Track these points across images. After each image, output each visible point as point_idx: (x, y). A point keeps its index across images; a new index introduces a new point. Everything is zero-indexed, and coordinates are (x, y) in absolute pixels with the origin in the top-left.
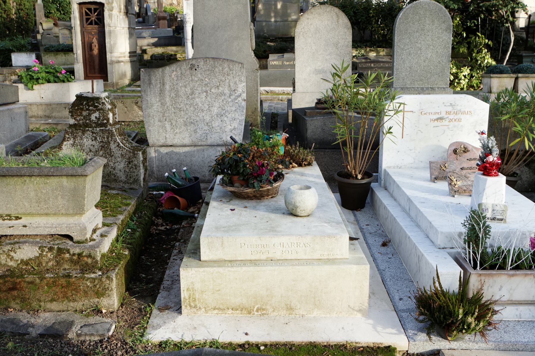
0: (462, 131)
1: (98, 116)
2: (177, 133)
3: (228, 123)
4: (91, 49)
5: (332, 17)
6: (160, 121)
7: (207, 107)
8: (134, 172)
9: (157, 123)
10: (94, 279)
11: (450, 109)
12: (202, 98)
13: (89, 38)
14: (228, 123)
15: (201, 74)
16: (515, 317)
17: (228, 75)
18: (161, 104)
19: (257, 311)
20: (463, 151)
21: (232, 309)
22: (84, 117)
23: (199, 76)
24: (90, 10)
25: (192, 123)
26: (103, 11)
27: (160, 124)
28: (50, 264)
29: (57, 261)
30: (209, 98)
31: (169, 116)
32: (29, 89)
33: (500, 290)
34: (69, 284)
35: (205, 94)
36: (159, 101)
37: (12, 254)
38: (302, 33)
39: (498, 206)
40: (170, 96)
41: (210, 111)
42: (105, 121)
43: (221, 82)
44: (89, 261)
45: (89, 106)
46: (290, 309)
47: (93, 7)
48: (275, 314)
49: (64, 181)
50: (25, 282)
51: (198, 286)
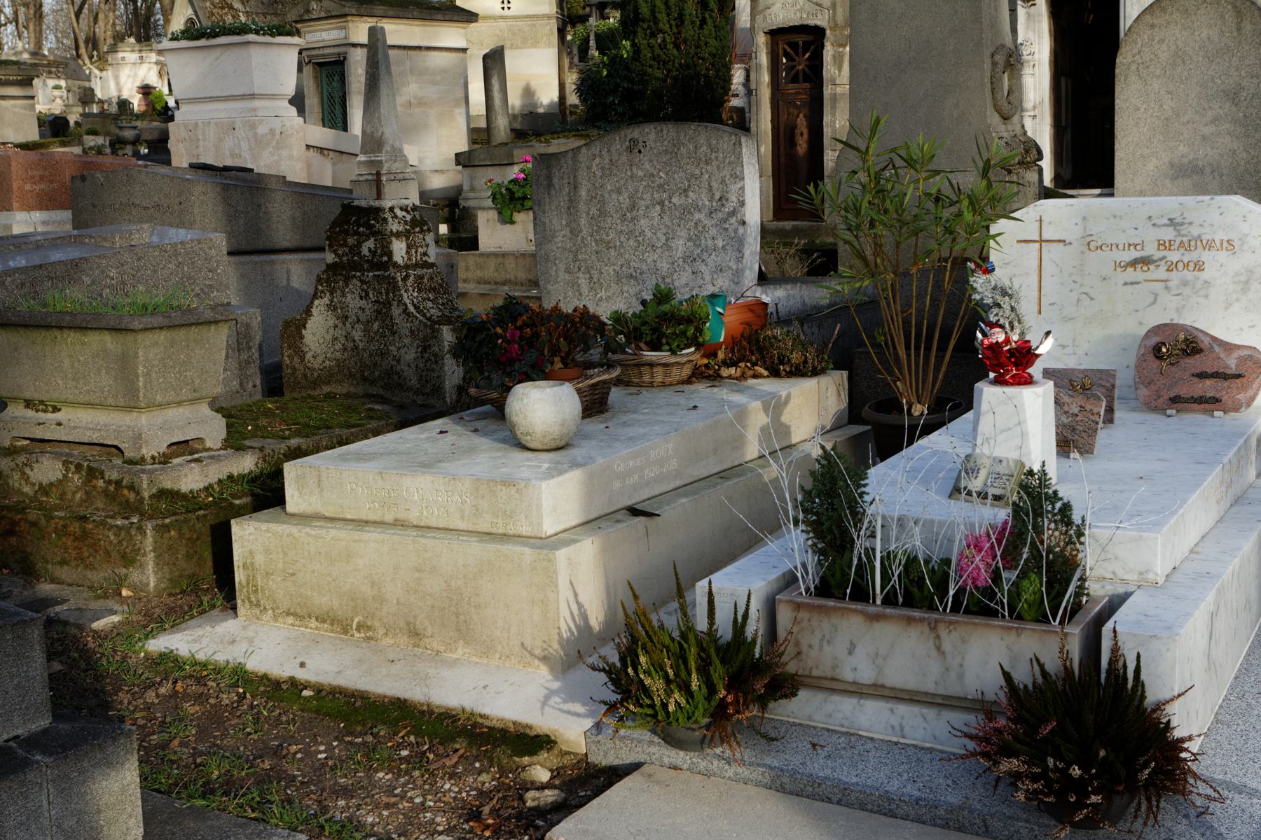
0: (1206, 296)
1: (372, 246)
2: (601, 299)
3: (708, 278)
4: (792, 143)
5: (1222, 16)
6: (568, 271)
7: (663, 239)
8: (433, 370)
9: (563, 276)
10: (119, 528)
11: (1168, 234)
12: (653, 218)
13: (789, 114)
14: (708, 278)
15: (651, 161)
16: (890, 731)
17: (707, 163)
18: (571, 232)
19: (358, 630)
20: (1183, 350)
21: (317, 619)
22: (351, 249)
23: (647, 166)
24: (794, 46)
25: (631, 276)
26: (823, 47)
27: (568, 277)
28: (78, 496)
29: (87, 493)
30: (666, 219)
31: (585, 260)
32: (506, 223)
33: (850, 653)
34: (85, 535)
35: (658, 208)
36: (568, 225)
37: (28, 471)
38: (1134, 67)
39: (1004, 463)
40: (588, 214)
41: (669, 248)
42: (385, 258)
43: (693, 181)
44: (132, 496)
45: (359, 226)
46: (415, 634)
47: (800, 39)
48: (389, 641)
49: (108, 340)
50: (26, 520)
51: (260, 559)
